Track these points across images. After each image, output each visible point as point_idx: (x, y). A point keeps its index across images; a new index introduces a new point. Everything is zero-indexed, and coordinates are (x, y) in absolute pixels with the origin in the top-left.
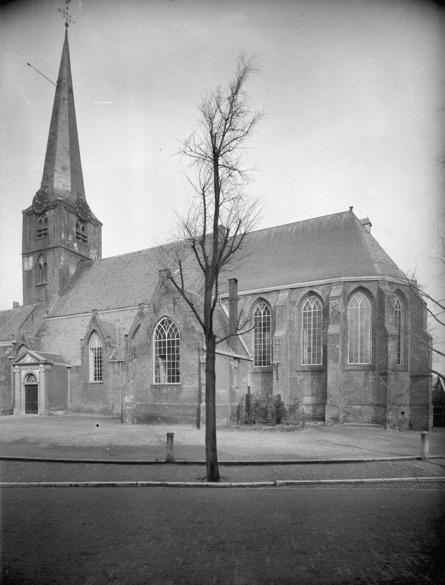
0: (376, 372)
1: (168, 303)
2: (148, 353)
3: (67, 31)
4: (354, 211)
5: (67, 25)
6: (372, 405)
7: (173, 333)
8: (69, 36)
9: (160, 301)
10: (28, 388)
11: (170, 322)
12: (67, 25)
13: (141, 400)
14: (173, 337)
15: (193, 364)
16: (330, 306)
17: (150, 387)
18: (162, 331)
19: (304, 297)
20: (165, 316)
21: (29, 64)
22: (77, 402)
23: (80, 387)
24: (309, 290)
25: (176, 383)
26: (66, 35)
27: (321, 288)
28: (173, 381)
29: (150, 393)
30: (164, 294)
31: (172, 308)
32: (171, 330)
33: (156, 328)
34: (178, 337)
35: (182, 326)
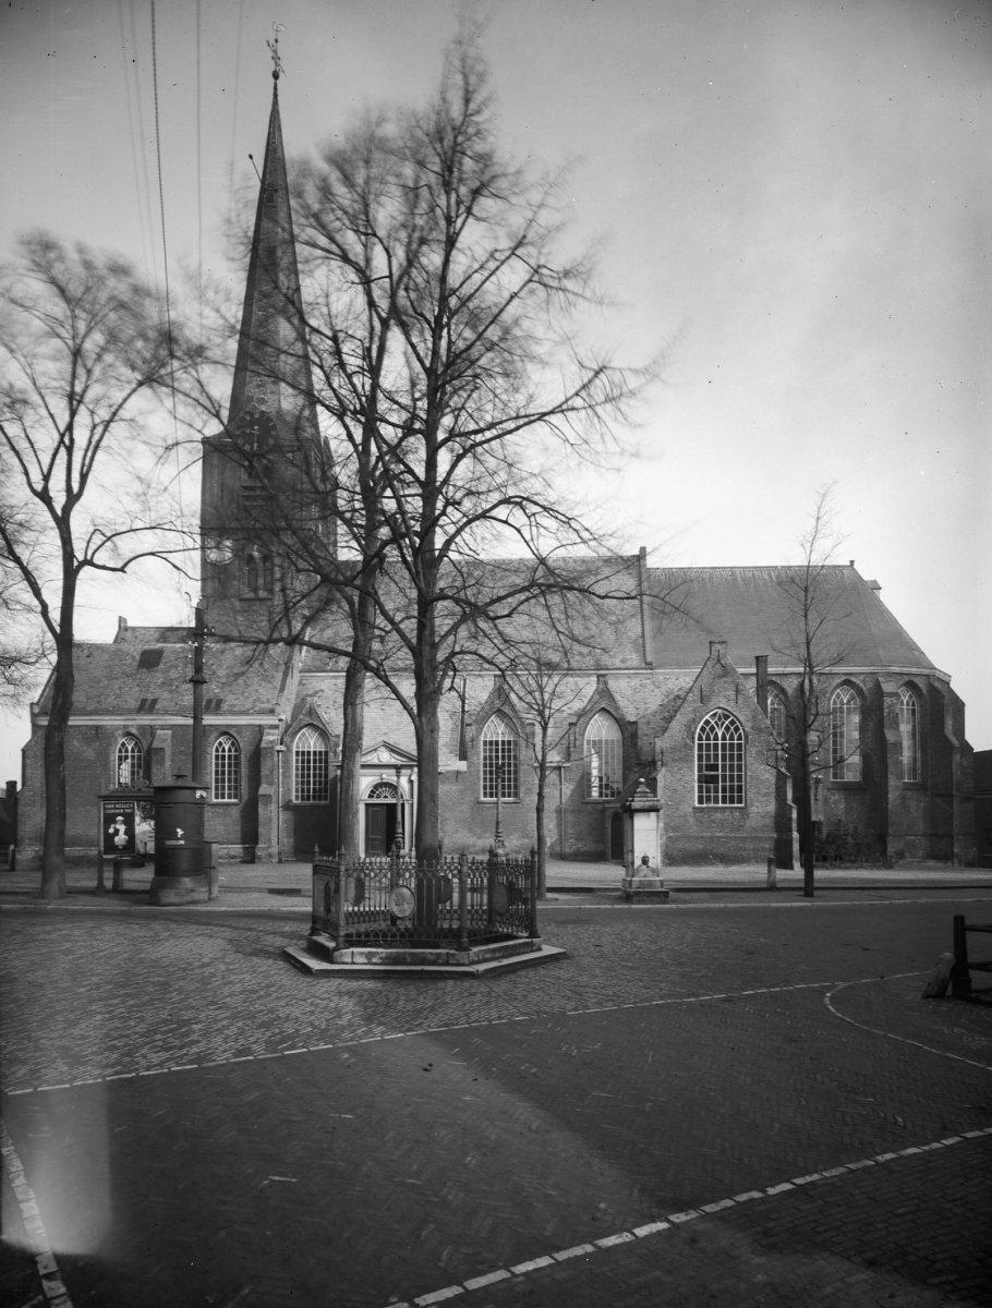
0: (929, 793)
1: (726, 690)
2: (687, 759)
3: (276, 89)
4: (855, 567)
5: (276, 76)
6: (924, 835)
7: (732, 734)
8: (279, 93)
9: (711, 685)
10: (371, 809)
11: (727, 717)
12: (276, 76)
13: (675, 829)
14: (732, 738)
15: (767, 779)
16: (886, 705)
17: (691, 810)
18: (712, 729)
19: (837, 686)
20: (719, 708)
21: (251, 157)
22: (457, 836)
23: (465, 808)
24: (844, 678)
25: (736, 805)
26: (275, 95)
27: (861, 677)
28: (732, 802)
29: (691, 820)
30: (720, 677)
31: (733, 697)
32: (727, 729)
33: (702, 723)
34: (740, 738)
35: (750, 724)
